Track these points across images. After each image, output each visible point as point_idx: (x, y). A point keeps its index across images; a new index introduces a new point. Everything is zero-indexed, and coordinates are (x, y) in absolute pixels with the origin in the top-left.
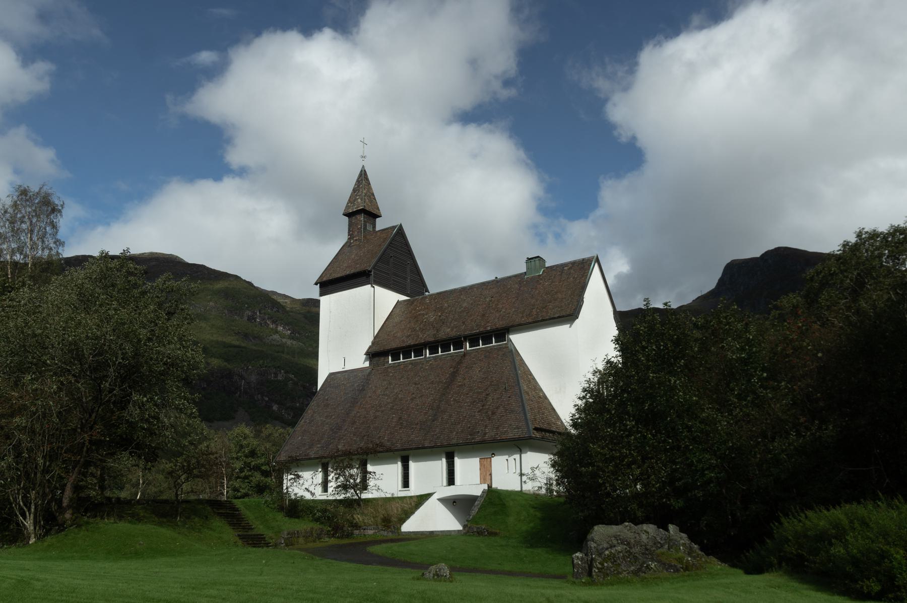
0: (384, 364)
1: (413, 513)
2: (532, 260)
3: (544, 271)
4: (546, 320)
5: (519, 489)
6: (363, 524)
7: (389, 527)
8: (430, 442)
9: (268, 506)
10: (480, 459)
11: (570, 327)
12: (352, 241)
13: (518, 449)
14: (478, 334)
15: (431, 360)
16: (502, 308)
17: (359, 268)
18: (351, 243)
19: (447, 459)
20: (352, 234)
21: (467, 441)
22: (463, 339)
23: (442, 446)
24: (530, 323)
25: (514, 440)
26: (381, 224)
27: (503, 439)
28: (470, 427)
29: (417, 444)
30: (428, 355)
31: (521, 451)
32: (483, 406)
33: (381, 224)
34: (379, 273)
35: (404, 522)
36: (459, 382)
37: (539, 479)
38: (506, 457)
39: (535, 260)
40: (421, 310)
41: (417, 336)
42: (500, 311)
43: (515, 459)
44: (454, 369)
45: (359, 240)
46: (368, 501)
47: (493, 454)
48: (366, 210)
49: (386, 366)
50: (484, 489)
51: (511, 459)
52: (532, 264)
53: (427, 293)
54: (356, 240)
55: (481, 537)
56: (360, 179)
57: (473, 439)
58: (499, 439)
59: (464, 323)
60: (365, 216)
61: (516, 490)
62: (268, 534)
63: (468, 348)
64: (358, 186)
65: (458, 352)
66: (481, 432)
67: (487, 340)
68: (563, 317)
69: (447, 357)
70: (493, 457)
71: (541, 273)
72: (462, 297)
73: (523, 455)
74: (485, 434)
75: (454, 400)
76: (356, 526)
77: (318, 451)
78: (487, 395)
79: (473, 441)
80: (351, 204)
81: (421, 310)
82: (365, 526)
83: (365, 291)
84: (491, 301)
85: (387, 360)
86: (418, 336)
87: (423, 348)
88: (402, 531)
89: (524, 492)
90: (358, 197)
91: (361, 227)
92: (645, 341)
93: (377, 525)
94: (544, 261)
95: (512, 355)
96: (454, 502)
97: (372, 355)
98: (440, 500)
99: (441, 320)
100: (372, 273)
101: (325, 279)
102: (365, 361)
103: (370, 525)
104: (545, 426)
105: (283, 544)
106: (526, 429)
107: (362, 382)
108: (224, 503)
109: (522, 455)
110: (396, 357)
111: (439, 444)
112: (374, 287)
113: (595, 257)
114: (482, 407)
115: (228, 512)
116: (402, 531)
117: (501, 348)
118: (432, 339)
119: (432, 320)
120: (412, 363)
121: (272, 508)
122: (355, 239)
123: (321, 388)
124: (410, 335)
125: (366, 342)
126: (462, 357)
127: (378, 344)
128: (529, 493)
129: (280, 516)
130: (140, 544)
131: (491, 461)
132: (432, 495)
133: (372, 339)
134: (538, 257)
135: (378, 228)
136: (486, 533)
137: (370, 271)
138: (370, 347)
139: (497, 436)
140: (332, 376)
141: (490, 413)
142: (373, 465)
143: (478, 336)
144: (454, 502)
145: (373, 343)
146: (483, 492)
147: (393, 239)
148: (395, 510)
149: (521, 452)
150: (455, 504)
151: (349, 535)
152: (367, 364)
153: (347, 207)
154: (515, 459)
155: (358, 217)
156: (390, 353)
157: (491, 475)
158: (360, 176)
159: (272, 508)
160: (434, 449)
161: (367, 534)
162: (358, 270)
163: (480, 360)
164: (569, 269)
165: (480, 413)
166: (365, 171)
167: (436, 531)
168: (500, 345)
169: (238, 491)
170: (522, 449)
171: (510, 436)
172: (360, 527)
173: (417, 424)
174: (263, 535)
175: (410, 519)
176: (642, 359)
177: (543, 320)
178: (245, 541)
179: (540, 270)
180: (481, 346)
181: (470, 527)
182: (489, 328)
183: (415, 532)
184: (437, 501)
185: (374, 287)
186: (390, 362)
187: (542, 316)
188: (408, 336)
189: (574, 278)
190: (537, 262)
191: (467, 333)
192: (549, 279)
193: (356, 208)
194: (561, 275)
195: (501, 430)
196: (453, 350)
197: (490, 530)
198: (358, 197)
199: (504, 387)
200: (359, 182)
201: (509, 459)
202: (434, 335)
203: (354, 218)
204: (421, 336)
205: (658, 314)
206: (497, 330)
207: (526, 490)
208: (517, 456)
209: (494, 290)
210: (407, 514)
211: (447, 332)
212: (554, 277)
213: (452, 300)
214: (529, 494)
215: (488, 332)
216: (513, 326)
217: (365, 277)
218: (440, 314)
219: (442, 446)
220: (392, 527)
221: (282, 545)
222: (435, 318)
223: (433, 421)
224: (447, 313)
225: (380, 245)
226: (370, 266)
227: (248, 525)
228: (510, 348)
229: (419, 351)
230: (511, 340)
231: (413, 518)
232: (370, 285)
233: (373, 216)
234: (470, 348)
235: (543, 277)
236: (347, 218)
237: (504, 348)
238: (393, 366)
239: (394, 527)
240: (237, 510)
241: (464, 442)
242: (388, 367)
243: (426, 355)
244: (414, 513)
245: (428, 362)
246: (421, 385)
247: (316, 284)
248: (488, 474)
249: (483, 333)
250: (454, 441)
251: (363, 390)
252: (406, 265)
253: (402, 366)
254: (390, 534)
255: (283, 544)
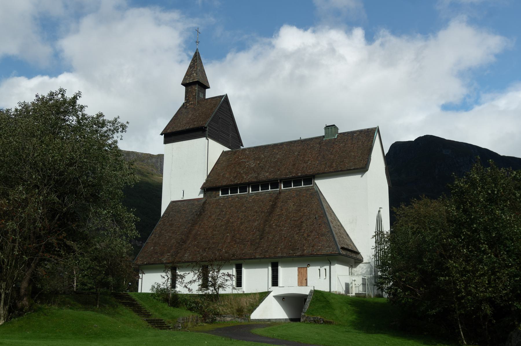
0: (216, 196)
1: (258, 306)
2: (329, 128)
3: (338, 136)
4: (345, 171)
5: (328, 290)
6: (223, 313)
7: (242, 315)
8: (260, 255)
9: (154, 298)
10: (298, 268)
11: (362, 177)
12: (188, 105)
13: (329, 262)
14: (301, 177)
15: (253, 195)
16: (308, 161)
17: (196, 125)
18: (187, 106)
19: (272, 267)
20: (188, 99)
21: (290, 255)
22: (279, 181)
23: (270, 258)
24: (332, 172)
25: (327, 255)
26: (210, 94)
27: (318, 255)
28: (291, 245)
29: (249, 256)
30: (250, 192)
31: (330, 264)
32: (299, 230)
33: (210, 94)
34: (212, 129)
35: (252, 312)
36: (278, 212)
37: (81, 278)
38: (319, 267)
39: (332, 127)
40: (243, 158)
41: (242, 177)
42: (307, 163)
43: (325, 269)
44: (273, 202)
45: (193, 104)
46: (223, 295)
47: (309, 265)
48: (199, 82)
49: (217, 198)
50: (311, 290)
51: (322, 269)
52: (329, 131)
53: (242, 147)
54: (191, 104)
55: (318, 324)
56: (195, 59)
57: (294, 253)
58: (315, 254)
59: (279, 170)
60: (199, 87)
61: (326, 291)
62: (166, 319)
63: (282, 188)
64: (194, 64)
65: (275, 191)
66: (300, 249)
67: (297, 182)
68: (357, 169)
69: (266, 194)
70: (308, 267)
71: (336, 137)
72: (275, 151)
73: (332, 267)
74: (304, 250)
75: (276, 225)
76: (218, 314)
77: (168, 258)
78: (302, 222)
79: (295, 255)
80: (188, 77)
81: (243, 158)
82: (225, 314)
83: (201, 142)
84: (298, 155)
85: (218, 194)
86: (243, 177)
87: (247, 186)
88: (251, 318)
89: (332, 292)
90: (194, 72)
91: (196, 95)
92: (480, 187)
93: (233, 314)
94: (337, 129)
95: (317, 195)
96: (283, 298)
97: (206, 189)
98: (274, 296)
99: (260, 167)
100: (207, 129)
101: (168, 131)
102: (200, 193)
103: (228, 314)
104: (346, 247)
105: (180, 327)
106: (336, 248)
107: (198, 209)
108: (123, 295)
109: (332, 267)
110: (225, 192)
111: (268, 256)
112: (208, 140)
113: (377, 129)
114: (299, 231)
115: (129, 302)
116: (251, 318)
117: (308, 189)
118: (255, 180)
119: (252, 166)
120: (237, 197)
121: (158, 300)
122: (190, 103)
123: (165, 213)
124: (236, 177)
125: (202, 179)
126: (278, 194)
127: (211, 182)
128: (336, 293)
129: (166, 306)
130: (95, 327)
131: (306, 270)
132: (270, 293)
133: (206, 177)
134: (334, 125)
135: (207, 97)
136: (322, 322)
137: (206, 128)
138: (204, 184)
139: (313, 252)
140: (173, 204)
141: (306, 235)
142: (246, 269)
143: (301, 178)
144: (283, 298)
145: (207, 181)
146: (310, 292)
147: (221, 106)
148: (245, 303)
149: (330, 264)
150: (284, 300)
151: (213, 321)
152: (202, 196)
153: (185, 79)
154: (325, 269)
155: (193, 87)
156: (220, 188)
157: (306, 279)
158: (195, 57)
159: (158, 300)
160: (262, 260)
161: (226, 320)
162: (196, 126)
163: (293, 197)
164: (358, 135)
165: (297, 235)
166: (198, 53)
167: (272, 319)
168: (307, 187)
169: (86, 285)
170: (331, 262)
171: (324, 252)
172: (221, 315)
173: (248, 241)
174: (162, 320)
175: (256, 310)
176: (482, 200)
177: (341, 171)
178: (154, 325)
179: (335, 135)
180: (292, 187)
181: (307, 317)
182: (300, 174)
183: (259, 319)
184: (273, 297)
185: (208, 140)
186: (220, 195)
187: (340, 168)
188: (235, 178)
189: (362, 142)
190: (333, 129)
191: (283, 177)
192: (343, 142)
193: (192, 80)
194: (352, 139)
195: (316, 248)
196: (239, 193)
197: (325, 320)
198: (194, 72)
199: (315, 217)
200: (194, 61)
201: (321, 269)
202: (256, 177)
203: (190, 87)
204: (245, 177)
205: (490, 168)
206: (306, 176)
207: (333, 291)
208: (327, 267)
209: (300, 147)
210: (253, 307)
211: (265, 176)
212: (347, 140)
213: (267, 153)
214: (336, 294)
215: (299, 177)
216: (318, 174)
217: (202, 132)
218: (258, 162)
219: (270, 258)
220: (244, 316)
221: (180, 328)
222: (255, 165)
223: (261, 239)
224: (264, 162)
225: (212, 109)
226: (206, 124)
227: (146, 312)
228: (316, 189)
229: (243, 188)
230: (316, 184)
231: (258, 309)
232: (205, 138)
233: (204, 86)
234: (283, 188)
235: (338, 140)
236: (184, 88)
237: (311, 189)
238: (223, 198)
239: (245, 315)
240: (134, 300)
241: (287, 255)
242: (219, 199)
243: (249, 191)
244: (258, 306)
245: (250, 196)
246: (247, 213)
247: (162, 134)
248: (304, 279)
249: (295, 178)
250: (280, 255)
251: (201, 214)
252: (229, 125)
253: (230, 199)
254: (243, 321)
255: (180, 327)
